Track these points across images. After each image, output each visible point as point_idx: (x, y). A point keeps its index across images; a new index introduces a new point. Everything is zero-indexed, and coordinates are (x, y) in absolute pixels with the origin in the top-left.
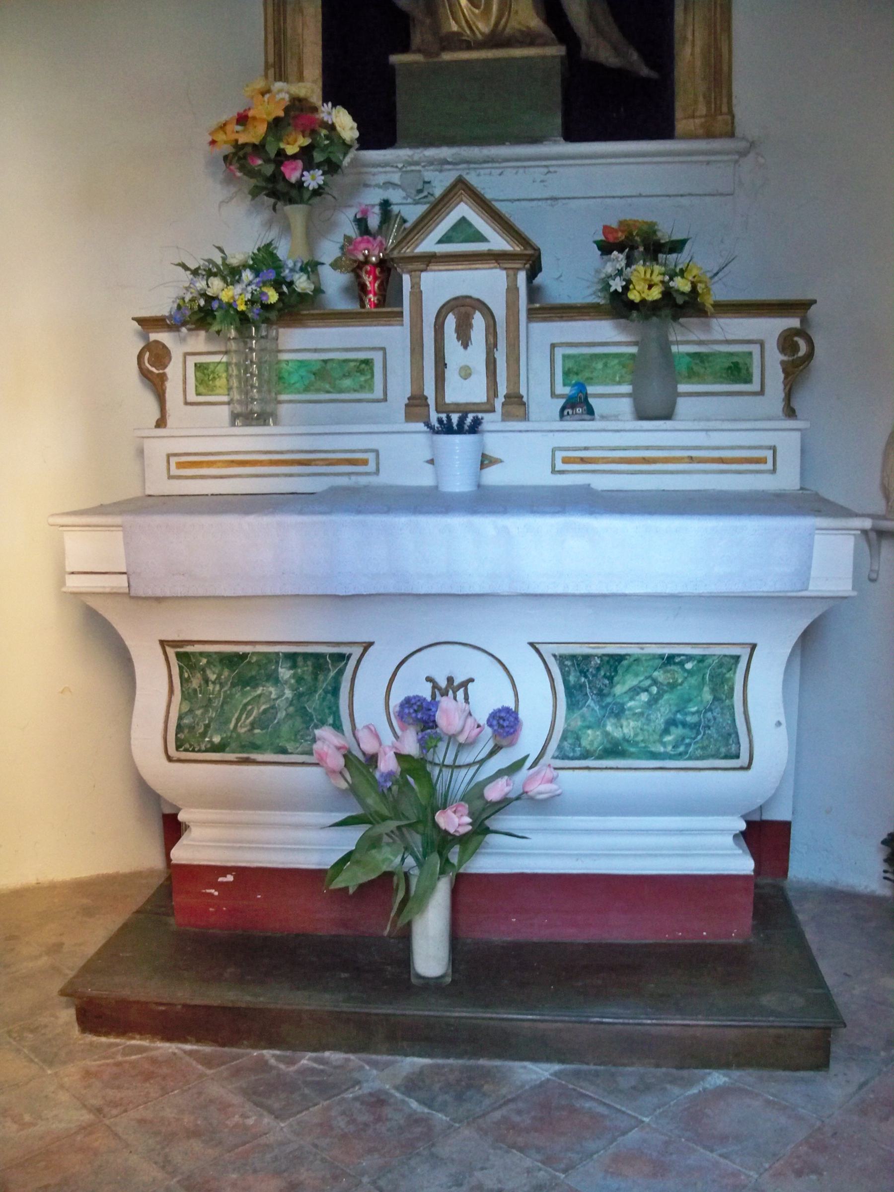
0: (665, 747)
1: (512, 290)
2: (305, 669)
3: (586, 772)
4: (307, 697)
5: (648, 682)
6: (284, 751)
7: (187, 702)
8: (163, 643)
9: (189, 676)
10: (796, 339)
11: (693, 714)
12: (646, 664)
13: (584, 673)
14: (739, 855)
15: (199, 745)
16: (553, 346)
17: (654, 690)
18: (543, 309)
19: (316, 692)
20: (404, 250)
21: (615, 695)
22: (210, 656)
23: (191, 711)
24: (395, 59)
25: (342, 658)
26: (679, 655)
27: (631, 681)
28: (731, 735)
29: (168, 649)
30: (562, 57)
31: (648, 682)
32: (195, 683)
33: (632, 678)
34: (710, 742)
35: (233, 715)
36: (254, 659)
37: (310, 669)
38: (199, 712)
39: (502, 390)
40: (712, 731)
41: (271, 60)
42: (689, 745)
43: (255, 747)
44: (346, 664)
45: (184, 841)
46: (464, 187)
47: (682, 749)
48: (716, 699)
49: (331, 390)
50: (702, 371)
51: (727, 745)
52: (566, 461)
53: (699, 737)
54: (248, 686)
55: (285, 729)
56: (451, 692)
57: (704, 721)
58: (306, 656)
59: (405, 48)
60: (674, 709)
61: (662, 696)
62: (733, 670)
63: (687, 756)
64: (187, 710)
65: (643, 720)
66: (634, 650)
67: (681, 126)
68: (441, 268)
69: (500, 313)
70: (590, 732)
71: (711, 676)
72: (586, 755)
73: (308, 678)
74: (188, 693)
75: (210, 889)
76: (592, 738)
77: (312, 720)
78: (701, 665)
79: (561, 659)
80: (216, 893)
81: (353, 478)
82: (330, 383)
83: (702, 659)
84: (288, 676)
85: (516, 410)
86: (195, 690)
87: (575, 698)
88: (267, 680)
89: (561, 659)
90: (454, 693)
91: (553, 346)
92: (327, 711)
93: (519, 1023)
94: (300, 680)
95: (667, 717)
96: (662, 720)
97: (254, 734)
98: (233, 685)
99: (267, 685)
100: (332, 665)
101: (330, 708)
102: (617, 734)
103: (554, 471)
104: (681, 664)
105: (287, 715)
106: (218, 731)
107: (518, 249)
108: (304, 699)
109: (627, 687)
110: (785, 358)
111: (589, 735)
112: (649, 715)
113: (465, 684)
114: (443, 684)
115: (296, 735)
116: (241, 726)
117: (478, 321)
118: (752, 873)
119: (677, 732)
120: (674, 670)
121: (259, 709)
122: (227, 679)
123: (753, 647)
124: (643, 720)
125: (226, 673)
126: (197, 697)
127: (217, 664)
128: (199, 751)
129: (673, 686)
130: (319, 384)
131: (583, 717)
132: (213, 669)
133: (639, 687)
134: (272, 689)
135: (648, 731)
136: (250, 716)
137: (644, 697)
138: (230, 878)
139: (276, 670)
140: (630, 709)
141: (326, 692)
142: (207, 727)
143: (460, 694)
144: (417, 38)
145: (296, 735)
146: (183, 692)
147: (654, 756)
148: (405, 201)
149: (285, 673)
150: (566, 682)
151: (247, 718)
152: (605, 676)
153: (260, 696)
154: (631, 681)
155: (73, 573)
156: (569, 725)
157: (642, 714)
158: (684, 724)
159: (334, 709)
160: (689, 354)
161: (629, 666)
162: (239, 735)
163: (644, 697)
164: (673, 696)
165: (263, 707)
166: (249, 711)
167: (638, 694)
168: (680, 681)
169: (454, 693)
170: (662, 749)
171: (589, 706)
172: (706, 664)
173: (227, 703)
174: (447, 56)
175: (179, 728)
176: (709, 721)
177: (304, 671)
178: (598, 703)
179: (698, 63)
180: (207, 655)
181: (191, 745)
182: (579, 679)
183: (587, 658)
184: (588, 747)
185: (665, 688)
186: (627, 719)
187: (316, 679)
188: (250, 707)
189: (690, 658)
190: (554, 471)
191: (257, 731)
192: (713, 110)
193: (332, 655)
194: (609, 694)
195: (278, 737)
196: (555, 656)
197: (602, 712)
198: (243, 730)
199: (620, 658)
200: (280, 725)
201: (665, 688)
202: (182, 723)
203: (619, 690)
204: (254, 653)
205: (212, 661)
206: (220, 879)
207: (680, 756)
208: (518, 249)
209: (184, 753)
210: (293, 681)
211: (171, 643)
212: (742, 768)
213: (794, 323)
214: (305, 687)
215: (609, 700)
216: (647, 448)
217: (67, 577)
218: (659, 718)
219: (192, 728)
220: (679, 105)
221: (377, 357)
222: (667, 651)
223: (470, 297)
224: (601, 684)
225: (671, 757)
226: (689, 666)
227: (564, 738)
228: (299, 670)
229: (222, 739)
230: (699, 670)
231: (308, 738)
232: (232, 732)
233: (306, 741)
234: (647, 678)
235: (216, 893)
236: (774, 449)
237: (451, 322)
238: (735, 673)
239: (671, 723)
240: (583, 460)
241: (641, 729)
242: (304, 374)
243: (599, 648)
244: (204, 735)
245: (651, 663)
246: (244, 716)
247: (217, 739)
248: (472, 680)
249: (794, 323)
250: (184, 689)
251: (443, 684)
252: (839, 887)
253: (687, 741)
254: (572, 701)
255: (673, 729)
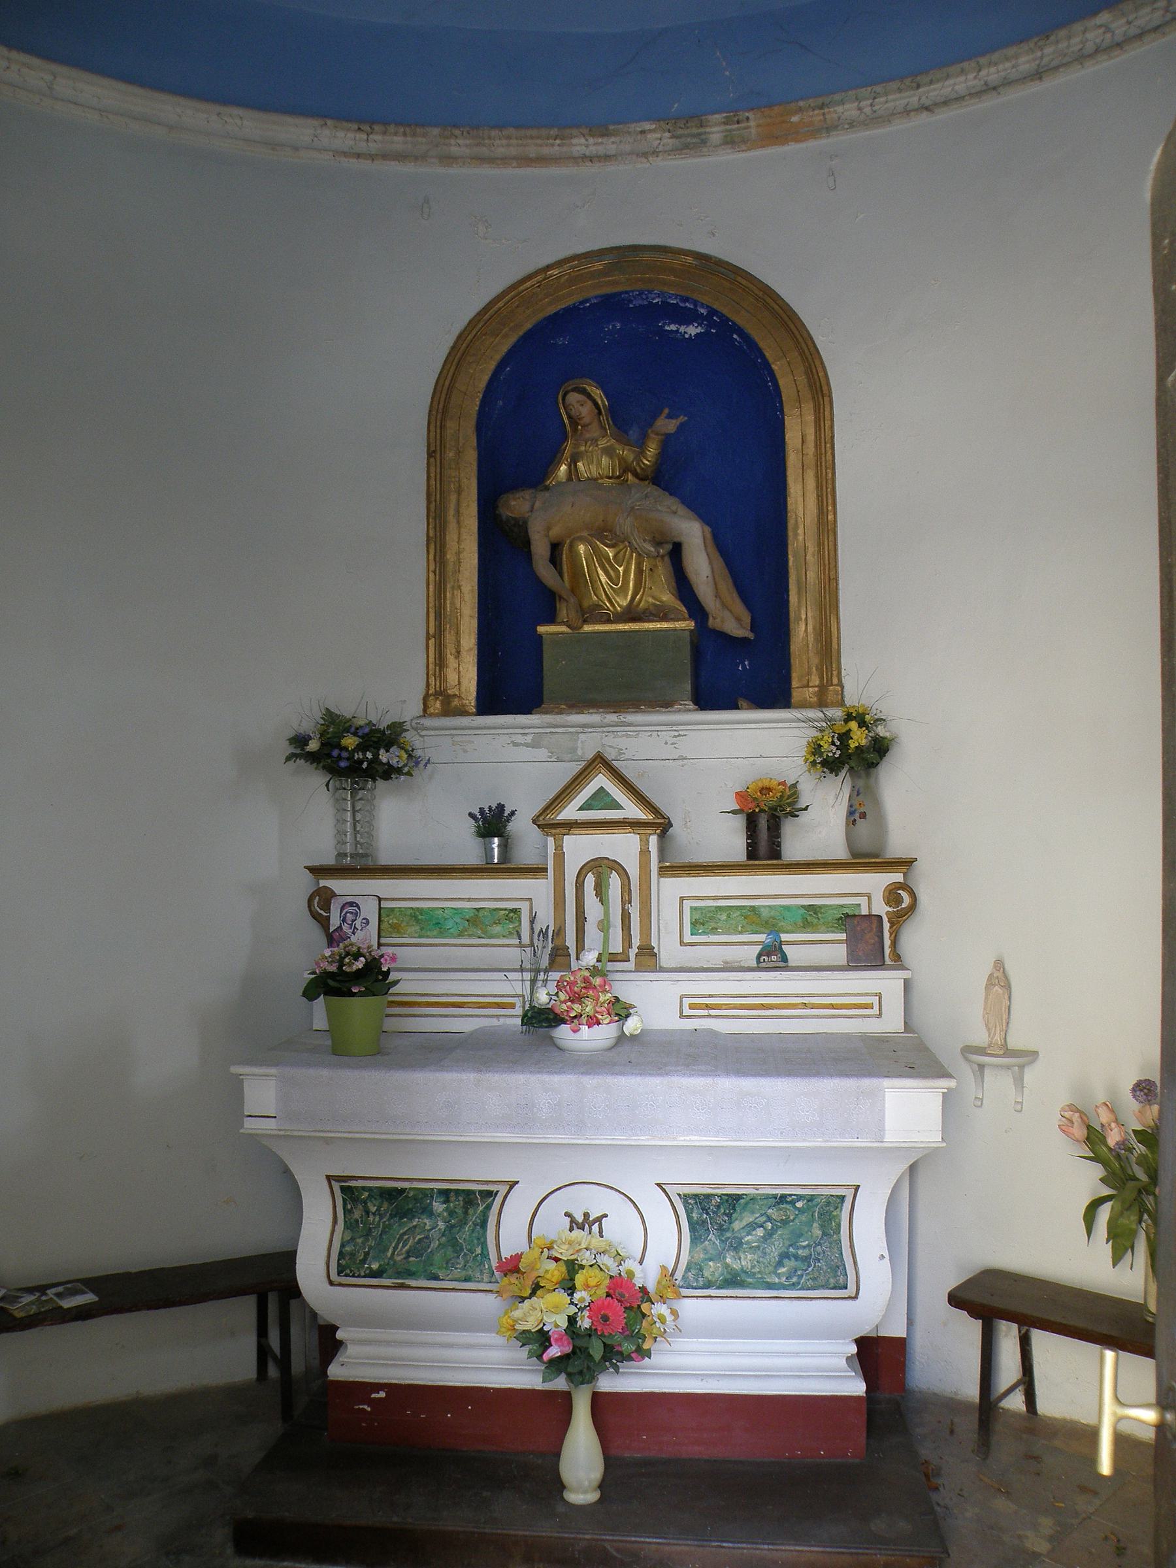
0: (779, 1278)
1: (644, 853)
2: (457, 1204)
3: (708, 1301)
4: (458, 1228)
5: (764, 1219)
6: (436, 1278)
7: (349, 1230)
8: (329, 1178)
9: (352, 1208)
10: (899, 892)
11: (804, 1247)
12: (761, 1203)
13: (705, 1210)
14: (853, 1376)
15: (359, 1271)
16: (682, 899)
17: (769, 1226)
18: (671, 867)
19: (466, 1224)
20: (549, 816)
21: (733, 1230)
22: (372, 1190)
23: (353, 1239)
24: (541, 629)
25: (490, 1194)
26: (790, 1195)
27: (748, 1218)
28: (838, 1268)
29: (333, 1183)
30: (691, 631)
31: (764, 1219)
32: (357, 1214)
33: (749, 1215)
34: (820, 1273)
35: (391, 1243)
36: (411, 1194)
37: (462, 1203)
38: (359, 1241)
39: (636, 942)
40: (822, 1264)
41: (432, 631)
42: (801, 1276)
43: (411, 1274)
44: (494, 1199)
45: (341, 1358)
46: (602, 761)
47: (794, 1280)
48: (824, 1234)
49: (483, 936)
50: (815, 921)
51: (835, 1276)
52: (692, 1007)
53: (810, 1269)
54: (406, 1218)
55: (437, 1258)
56: (587, 1226)
57: (815, 1255)
58: (458, 1192)
59: (552, 619)
60: (787, 1243)
61: (776, 1231)
62: (840, 1208)
63: (800, 1286)
64: (349, 1238)
65: (759, 1253)
66: (750, 1191)
67: (796, 695)
68: (581, 832)
69: (634, 872)
70: (711, 1263)
71: (820, 1214)
72: (708, 1285)
73: (459, 1211)
74: (351, 1223)
75: (364, 1404)
76: (713, 1269)
77: (462, 1250)
78: (810, 1203)
79: (685, 1198)
80: (369, 1409)
81: (502, 1020)
82: (481, 929)
83: (811, 1199)
84: (441, 1210)
85: (646, 960)
86: (357, 1221)
87: (698, 1232)
88: (423, 1213)
89: (685, 1198)
90: (590, 1227)
91: (682, 899)
92: (475, 1241)
93: (640, 1545)
94: (452, 1213)
95: (781, 1251)
96: (776, 1253)
97: (409, 1262)
98: (392, 1216)
99: (423, 1217)
100: (481, 1200)
101: (479, 1239)
102: (736, 1266)
103: (682, 1016)
104: (793, 1203)
105: (440, 1244)
106: (375, 1258)
107: (651, 817)
108: (455, 1230)
109: (744, 1223)
110: (891, 909)
111: (710, 1267)
112: (764, 1248)
113: (599, 1220)
114: (580, 1219)
115: (447, 1263)
116: (397, 1254)
117: (615, 880)
118: (865, 1395)
119: (790, 1264)
120: (786, 1209)
121: (414, 1239)
122: (386, 1211)
123: (857, 1188)
124: (759, 1253)
125: (385, 1205)
126: (359, 1226)
127: (378, 1197)
128: (359, 1276)
129: (785, 1222)
130: (473, 930)
131: (705, 1250)
132: (374, 1202)
133: (755, 1223)
134: (426, 1221)
135: (764, 1264)
136: (406, 1246)
137: (760, 1232)
138: (382, 1394)
139: (431, 1204)
140: (748, 1243)
141: (475, 1225)
142: (367, 1254)
143: (595, 1227)
144: (563, 612)
145: (447, 1263)
146: (345, 1222)
147: (770, 1286)
148: (549, 760)
149: (438, 1207)
150: (689, 1218)
151: (403, 1247)
152: (724, 1214)
153: (415, 1227)
154: (748, 1218)
155: (250, 1116)
156: (692, 1257)
157: (758, 1247)
158: (796, 1257)
159: (482, 1239)
160: (803, 907)
161: (747, 1204)
162: (395, 1262)
163: (760, 1232)
164: (786, 1232)
165: (419, 1237)
166: (406, 1240)
167: (754, 1229)
168: (792, 1218)
169: (590, 1227)
170: (777, 1280)
171: (710, 1240)
172: (814, 1203)
173: (386, 1232)
174: (587, 628)
175: (341, 1255)
176: (819, 1254)
177: (456, 1205)
178: (719, 1237)
179: (811, 638)
180: (370, 1189)
181: (351, 1271)
182: (701, 1215)
183: (708, 1197)
184: (710, 1278)
185: (779, 1224)
186: (745, 1252)
187: (466, 1213)
188: (406, 1237)
189: (800, 1197)
190: (682, 1016)
191: (412, 1259)
192: (825, 681)
193: (481, 1192)
194: (727, 1230)
195: (432, 1265)
196: (679, 1195)
197: (723, 1245)
198: (398, 1258)
199: (738, 1197)
200: (433, 1254)
201: (779, 1224)
202: (343, 1250)
203: (737, 1225)
204: (411, 1189)
205: (373, 1194)
206: (373, 1396)
207: (793, 1286)
208: (651, 817)
209: (345, 1277)
210: (445, 1214)
211: (336, 1178)
212: (850, 1298)
213: (898, 877)
214: (456, 1219)
215: (728, 1234)
216: (765, 996)
217: (246, 1119)
218: (774, 1251)
219: (352, 1255)
220: (795, 675)
221: (524, 907)
222: (779, 1192)
223: (608, 859)
224: (721, 1220)
225: (785, 1288)
226: (799, 1205)
227: (688, 1269)
228: (452, 1205)
229: (380, 1266)
230: (809, 1208)
231: (458, 1266)
232: (390, 1259)
233: (456, 1268)
234: (762, 1215)
235: (369, 1409)
236: (880, 996)
237: (590, 880)
238: (841, 1210)
239: (785, 1256)
240: (708, 1007)
241: (757, 1262)
242: (459, 921)
243: (719, 1188)
244: (364, 1261)
245: (765, 1201)
246: (401, 1245)
247: (375, 1266)
248: (606, 1216)
249: (898, 877)
250: (347, 1220)
251: (580, 1219)
252: (959, 1397)
253: (799, 1273)
254: (695, 1235)
255: (786, 1261)
